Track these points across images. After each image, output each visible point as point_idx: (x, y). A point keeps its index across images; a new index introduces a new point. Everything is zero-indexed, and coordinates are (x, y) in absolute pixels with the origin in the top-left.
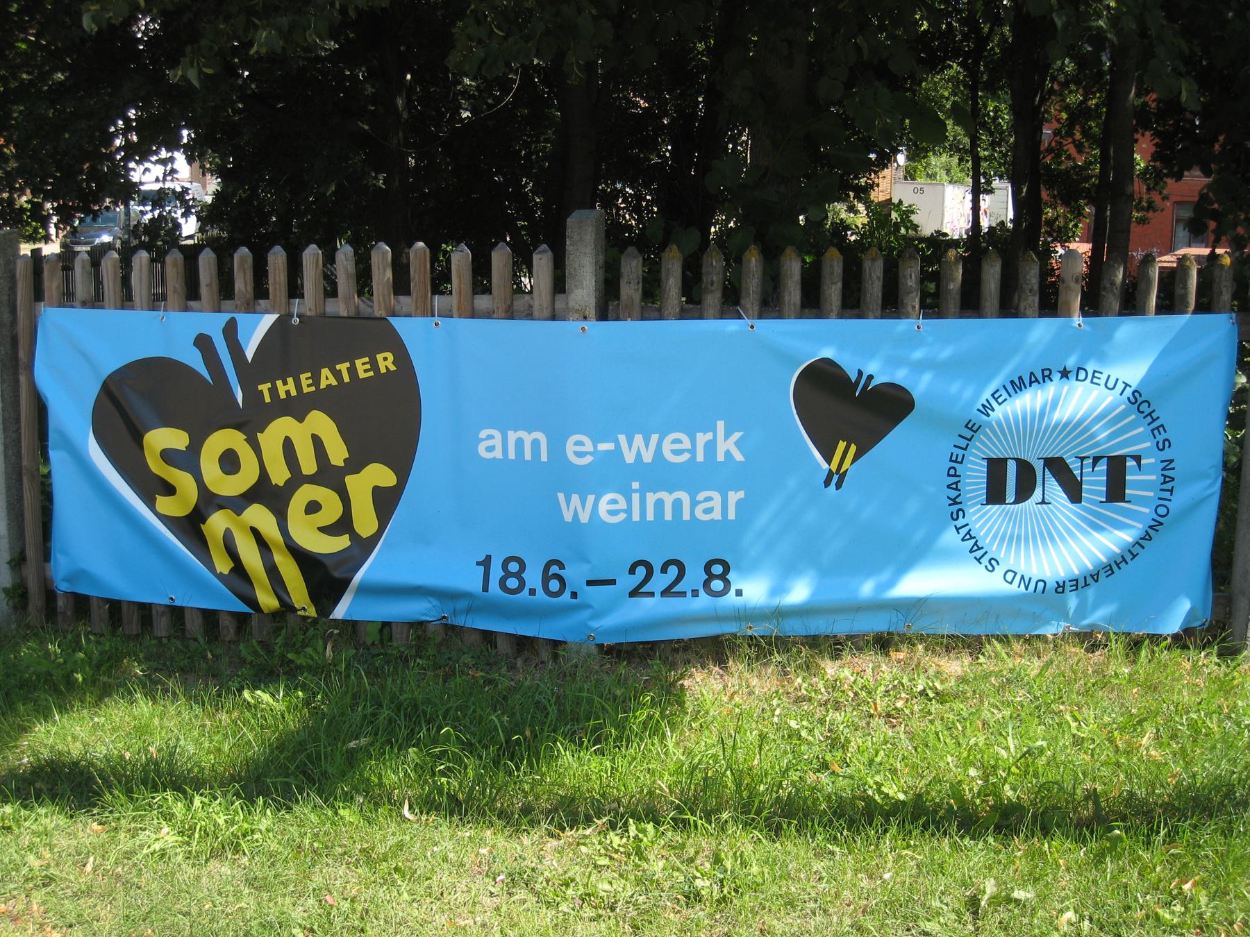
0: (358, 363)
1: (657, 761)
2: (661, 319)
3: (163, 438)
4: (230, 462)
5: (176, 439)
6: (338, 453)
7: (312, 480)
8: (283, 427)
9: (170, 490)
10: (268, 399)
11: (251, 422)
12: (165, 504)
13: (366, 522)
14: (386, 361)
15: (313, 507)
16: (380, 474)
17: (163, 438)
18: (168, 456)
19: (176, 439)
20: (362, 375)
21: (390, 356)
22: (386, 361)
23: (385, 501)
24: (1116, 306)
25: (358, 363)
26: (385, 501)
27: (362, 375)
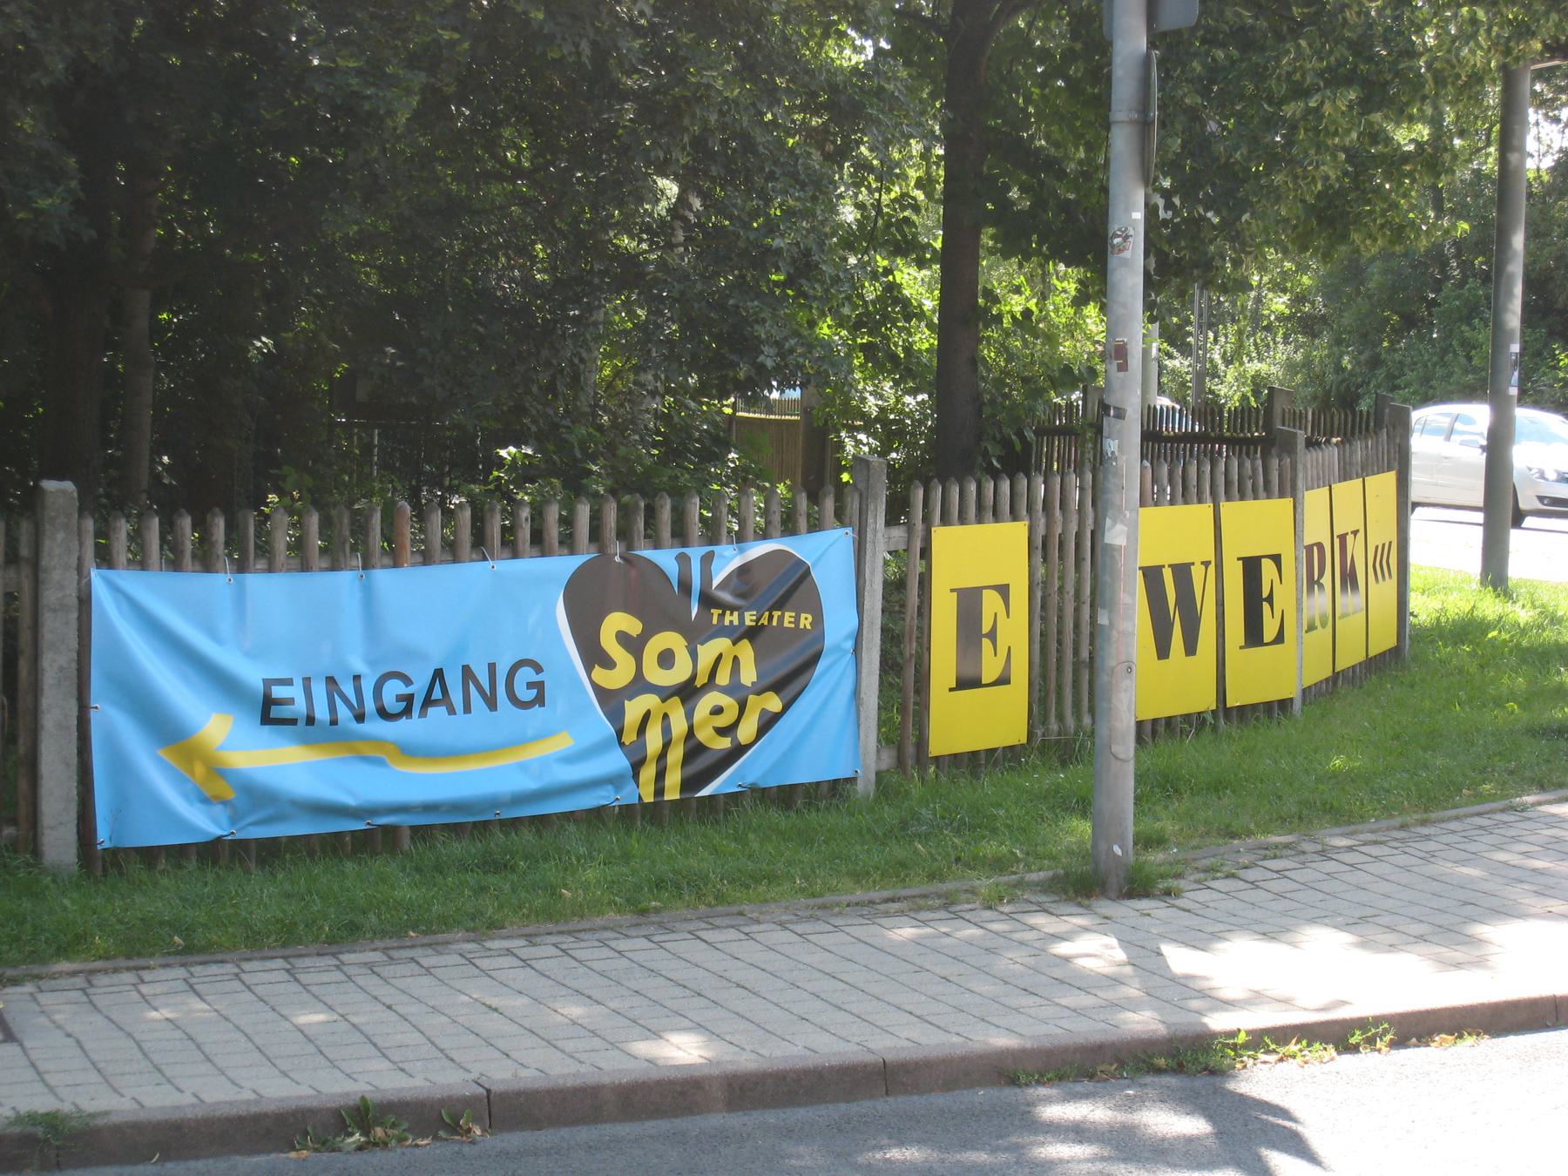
0: (787, 614)
1: (1178, 902)
2: (454, 561)
3: (618, 622)
4: (666, 659)
5: (633, 626)
6: (749, 676)
7: (726, 690)
8: (721, 644)
9: (608, 663)
10: (715, 621)
11: (695, 635)
12: (599, 674)
13: (746, 731)
14: (806, 621)
15: (717, 711)
16: (774, 703)
17: (618, 622)
18: (623, 638)
19: (633, 626)
20: (786, 624)
21: (810, 618)
22: (806, 621)
23: (768, 723)
24: (157, 565)
25: (787, 614)
26: (768, 723)
27: (786, 624)
